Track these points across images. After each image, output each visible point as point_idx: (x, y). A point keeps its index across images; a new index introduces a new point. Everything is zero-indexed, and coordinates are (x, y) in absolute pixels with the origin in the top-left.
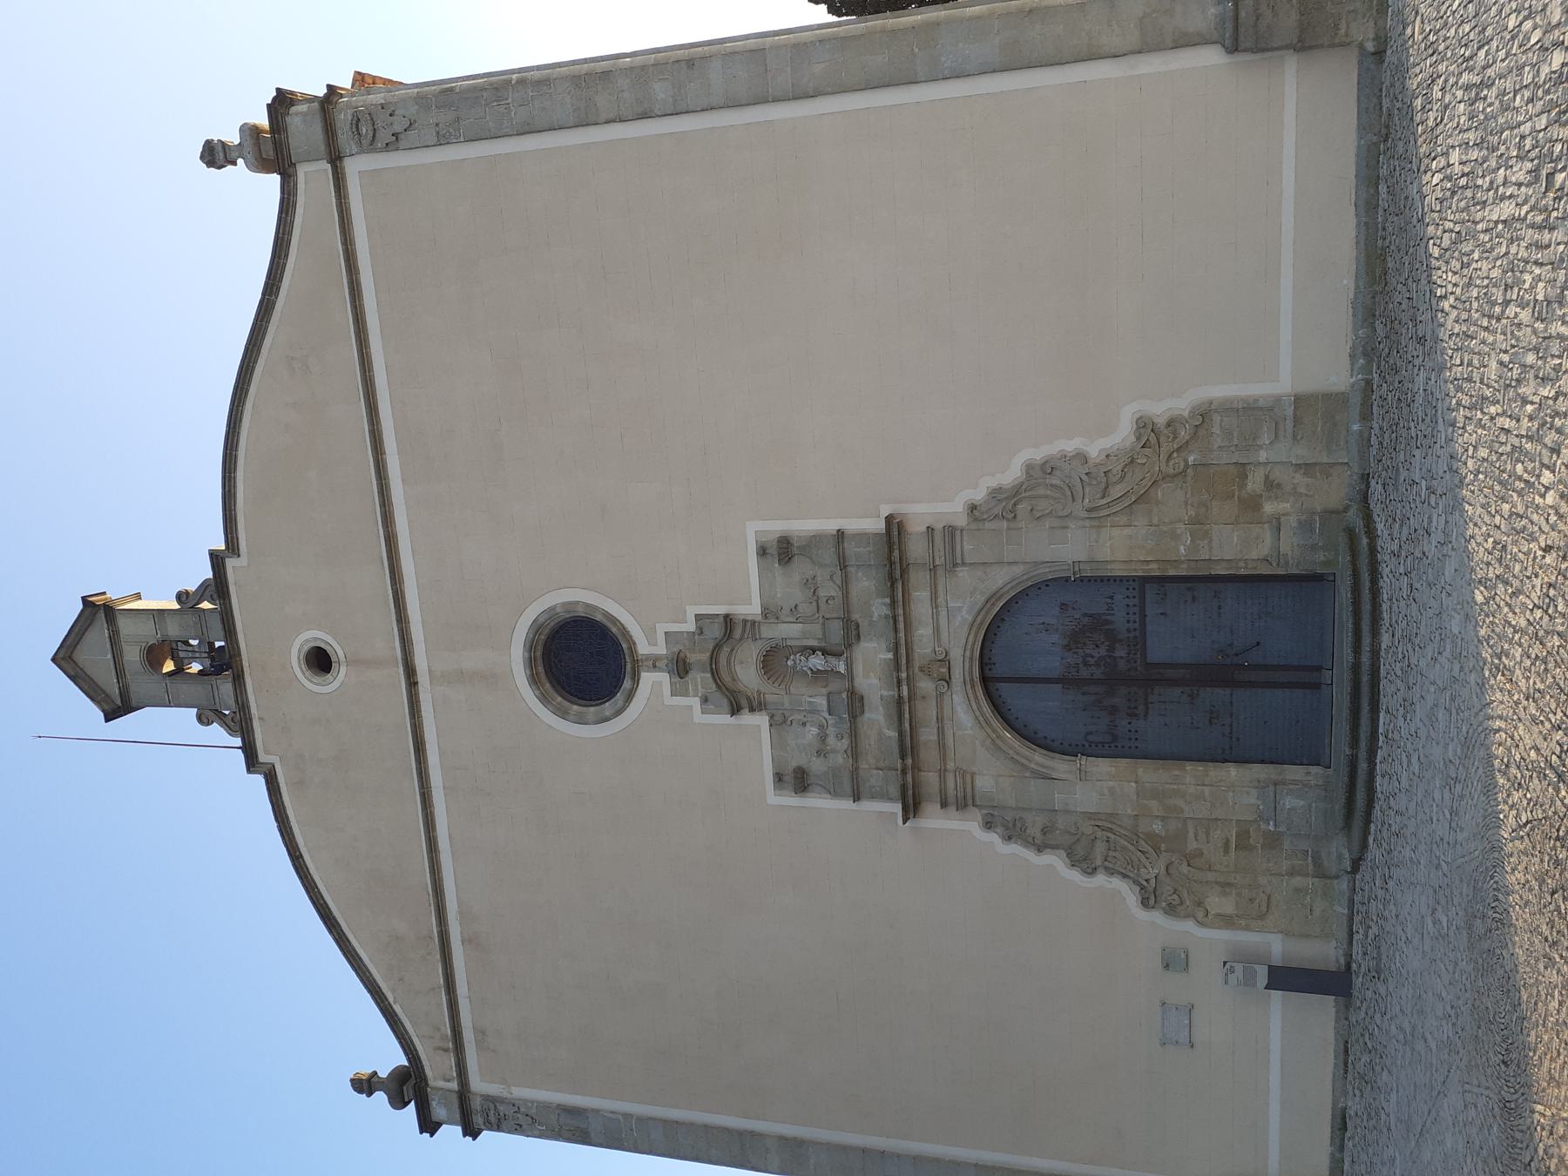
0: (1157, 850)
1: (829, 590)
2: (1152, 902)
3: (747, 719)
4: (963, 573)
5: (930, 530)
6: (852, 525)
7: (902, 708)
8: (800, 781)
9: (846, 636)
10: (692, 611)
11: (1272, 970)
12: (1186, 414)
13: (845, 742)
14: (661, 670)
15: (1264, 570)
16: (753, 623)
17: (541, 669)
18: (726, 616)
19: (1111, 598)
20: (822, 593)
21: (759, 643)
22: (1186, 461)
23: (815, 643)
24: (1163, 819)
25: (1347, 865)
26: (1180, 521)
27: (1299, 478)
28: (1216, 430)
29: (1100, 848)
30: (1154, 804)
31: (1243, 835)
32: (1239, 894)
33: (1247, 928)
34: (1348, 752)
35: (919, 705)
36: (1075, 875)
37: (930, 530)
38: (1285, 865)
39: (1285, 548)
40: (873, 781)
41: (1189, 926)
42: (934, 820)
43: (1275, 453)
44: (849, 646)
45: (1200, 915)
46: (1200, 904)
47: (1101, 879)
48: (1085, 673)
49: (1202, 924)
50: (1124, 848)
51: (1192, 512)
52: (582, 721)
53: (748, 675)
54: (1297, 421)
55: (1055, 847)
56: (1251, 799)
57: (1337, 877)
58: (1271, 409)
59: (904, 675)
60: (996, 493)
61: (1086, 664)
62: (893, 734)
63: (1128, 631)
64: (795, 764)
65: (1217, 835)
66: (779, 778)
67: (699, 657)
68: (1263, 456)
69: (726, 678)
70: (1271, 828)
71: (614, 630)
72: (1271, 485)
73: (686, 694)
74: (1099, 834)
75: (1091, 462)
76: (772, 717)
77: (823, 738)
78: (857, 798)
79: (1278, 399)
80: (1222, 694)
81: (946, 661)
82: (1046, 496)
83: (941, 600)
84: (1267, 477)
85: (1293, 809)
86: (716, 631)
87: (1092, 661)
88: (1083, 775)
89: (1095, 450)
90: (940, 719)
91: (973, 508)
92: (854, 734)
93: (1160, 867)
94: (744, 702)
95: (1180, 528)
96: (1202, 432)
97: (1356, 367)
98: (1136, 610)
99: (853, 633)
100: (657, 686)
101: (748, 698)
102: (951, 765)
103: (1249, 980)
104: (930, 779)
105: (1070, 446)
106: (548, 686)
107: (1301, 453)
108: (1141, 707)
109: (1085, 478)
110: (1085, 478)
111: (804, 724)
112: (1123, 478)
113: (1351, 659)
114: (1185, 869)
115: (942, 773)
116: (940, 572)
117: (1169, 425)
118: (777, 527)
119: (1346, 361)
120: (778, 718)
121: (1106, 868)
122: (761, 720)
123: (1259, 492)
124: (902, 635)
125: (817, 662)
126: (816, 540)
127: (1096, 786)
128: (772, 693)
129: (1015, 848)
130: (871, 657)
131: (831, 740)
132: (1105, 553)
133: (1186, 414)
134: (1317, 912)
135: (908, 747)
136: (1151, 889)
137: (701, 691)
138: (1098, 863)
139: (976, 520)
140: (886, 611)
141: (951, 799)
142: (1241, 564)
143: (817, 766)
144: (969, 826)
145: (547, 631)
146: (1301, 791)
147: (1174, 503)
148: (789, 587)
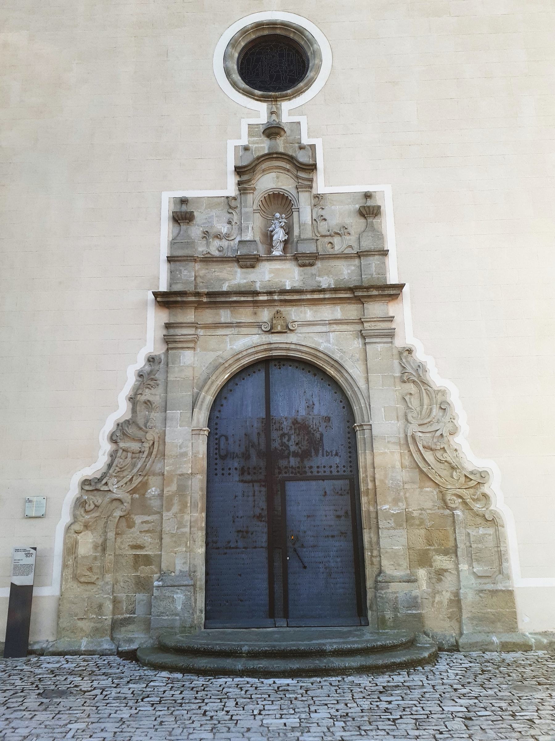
0: (134, 491)
1: (339, 245)
2: (87, 488)
3: (232, 180)
4: (358, 343)
5: (391, 319)
6: (392, 261)
7: (249, 297)
8: (182, 216)
9: (305, 255)
10: (318, 142)
11: (29, 589)
12: (492, 508)
13: (216, 253)
14: (269, 117)
15: (370, 572)
16: (311, 187)
17: (266, 33)
18: (315, 165)
19: (337, 454)
20: (336, 240)
21: (294, 192)
22: (456, 509)
23: (296, 232)
24: (161, 496)
25: (125, 647)
26: (408, 505)
27: (447, 596)
28: (481, 531)
29: (135, 446)
30: (174, 487)
31: (147, 560)
32: (95, 558)
33: (65, 566)
34: (245, 649)
35: (249, 310)
36: (109, 426)
37: (391, 319)
38: (122, 596)
39: (394, 587)
40: (185, 273)
41: (66, 518)
42: (154, 320)
43: (467, 577)
44: (296, 258)
45: (77, 527)
46: (86, 526)
47: (107, 447)
48: (275, 435)
49: (68, 529)
50: (134, 465)
51: (415, 514)
52: (226, 58)
53: (268, 181)
54: (494, 593)
55: (134, 411)
56: (180, 566)
57: (112, 639)
58: (501, 572)
59: (276, 297)
60: (420, 367)
61: (283, 435)
62: (225, 288)
63: (311, 467)
64: (196, 214)
65: (147, 539)
66: (184, 201)
67: (281, 145)
68: (464, 567)
69: (264, 166)
70: (156, 583)
71: (301, 84)
72: (440, 574)
73: (250, 135)
74: (147, 445)
75: (450, 438)
76: (235, 199)
77: (218, 236)
78: (170, 259)
79: (508, 578)
80: (263, 540)
81: (287, 330)
82: (422, 405)
83: (335, 327)
84: (446, 571)
85: (174, 600)
86: (303, 157)
87: (285, 440)
88: (196, 432)
89: (459, 440)
90: (239, 325)
91: (410, 351)
92: (223, 260)
93: (119, 494)
94: (245, 178)
95: (402, 505)
96: (479, 520)
97: (539, 637)
98: (328, 473)
99: (305, 260)
100: (257, 114)
101: (249, 181)
102: (201, 332)
103: (18, 569)
104: (190, 316)
105: (462, 422)
106: (253, 37)
107: (469, 597)
108: (249, 478)
109: (438, 433)
110: (438, 433)
111: (229, 223)
112: (440, 461)
113: (328, 648)
114: (118, 513)
115: (195, 325)
116: (359, 327)
117: (485, 495)
118: (388, 209)
119: (541, 629)
120: (233, 203)
121: (117, 451)
122: (231, 190)
123: (434, 564)
124: (309, 296)
125: (280, 235)
126: (380, 236)
127: (186, 442)
128: (253, 200)
129: (131, 380)
130: (290, 275)
131: (216, 243)
132: (379, 448)
133: (492, 508)
134: (80, 624)
135: (216, 299)
136: (99, 486)
137: (253, 146)
138: (122, 445)
139: (400, 353)
140: (324, 286)
141: (172, 331)
142: (375, 553)
143: (195, 231)
144: (151, 343)
145: (296, 38)
146: (185, 605)
147: (422, 500)
148: (341, 214)
